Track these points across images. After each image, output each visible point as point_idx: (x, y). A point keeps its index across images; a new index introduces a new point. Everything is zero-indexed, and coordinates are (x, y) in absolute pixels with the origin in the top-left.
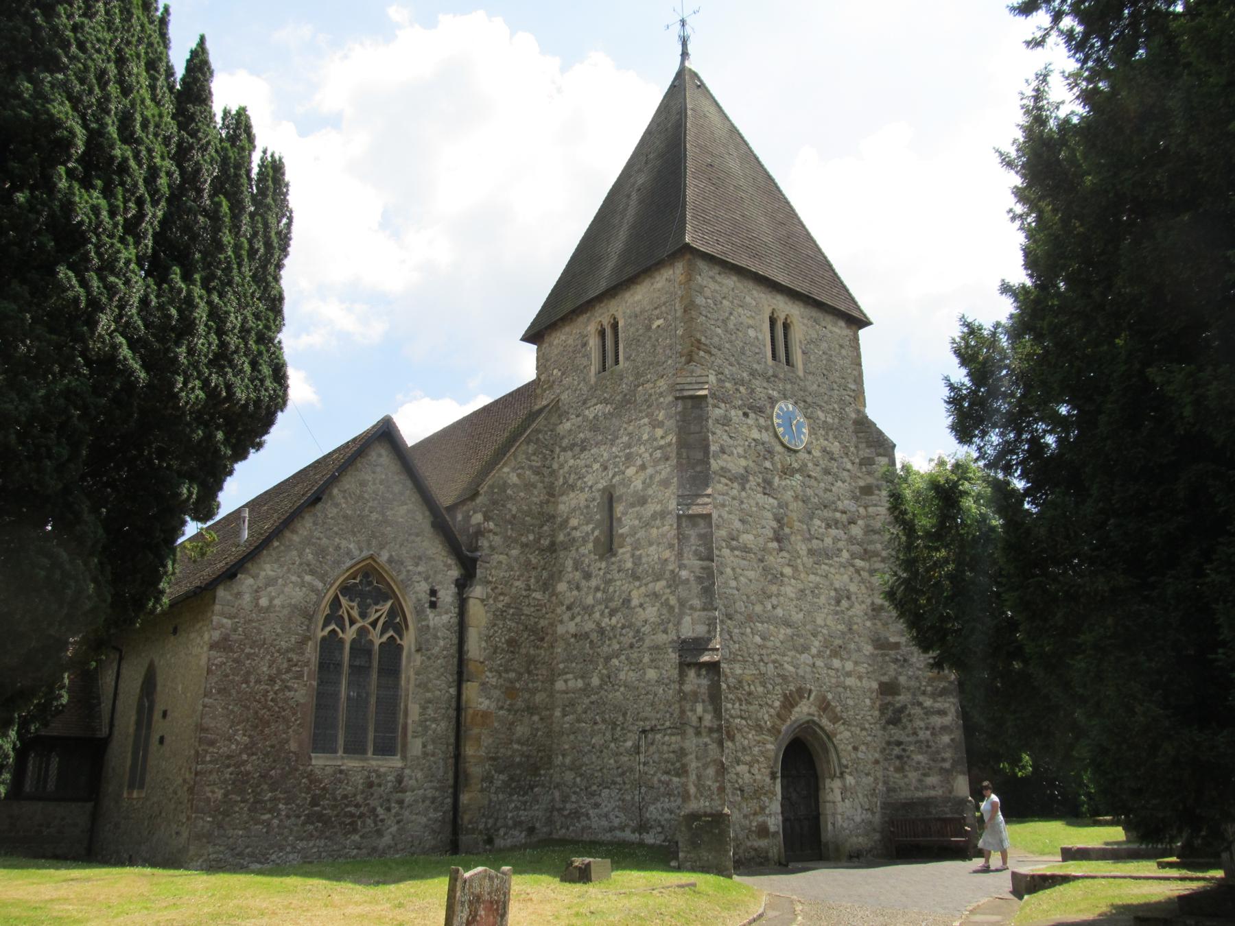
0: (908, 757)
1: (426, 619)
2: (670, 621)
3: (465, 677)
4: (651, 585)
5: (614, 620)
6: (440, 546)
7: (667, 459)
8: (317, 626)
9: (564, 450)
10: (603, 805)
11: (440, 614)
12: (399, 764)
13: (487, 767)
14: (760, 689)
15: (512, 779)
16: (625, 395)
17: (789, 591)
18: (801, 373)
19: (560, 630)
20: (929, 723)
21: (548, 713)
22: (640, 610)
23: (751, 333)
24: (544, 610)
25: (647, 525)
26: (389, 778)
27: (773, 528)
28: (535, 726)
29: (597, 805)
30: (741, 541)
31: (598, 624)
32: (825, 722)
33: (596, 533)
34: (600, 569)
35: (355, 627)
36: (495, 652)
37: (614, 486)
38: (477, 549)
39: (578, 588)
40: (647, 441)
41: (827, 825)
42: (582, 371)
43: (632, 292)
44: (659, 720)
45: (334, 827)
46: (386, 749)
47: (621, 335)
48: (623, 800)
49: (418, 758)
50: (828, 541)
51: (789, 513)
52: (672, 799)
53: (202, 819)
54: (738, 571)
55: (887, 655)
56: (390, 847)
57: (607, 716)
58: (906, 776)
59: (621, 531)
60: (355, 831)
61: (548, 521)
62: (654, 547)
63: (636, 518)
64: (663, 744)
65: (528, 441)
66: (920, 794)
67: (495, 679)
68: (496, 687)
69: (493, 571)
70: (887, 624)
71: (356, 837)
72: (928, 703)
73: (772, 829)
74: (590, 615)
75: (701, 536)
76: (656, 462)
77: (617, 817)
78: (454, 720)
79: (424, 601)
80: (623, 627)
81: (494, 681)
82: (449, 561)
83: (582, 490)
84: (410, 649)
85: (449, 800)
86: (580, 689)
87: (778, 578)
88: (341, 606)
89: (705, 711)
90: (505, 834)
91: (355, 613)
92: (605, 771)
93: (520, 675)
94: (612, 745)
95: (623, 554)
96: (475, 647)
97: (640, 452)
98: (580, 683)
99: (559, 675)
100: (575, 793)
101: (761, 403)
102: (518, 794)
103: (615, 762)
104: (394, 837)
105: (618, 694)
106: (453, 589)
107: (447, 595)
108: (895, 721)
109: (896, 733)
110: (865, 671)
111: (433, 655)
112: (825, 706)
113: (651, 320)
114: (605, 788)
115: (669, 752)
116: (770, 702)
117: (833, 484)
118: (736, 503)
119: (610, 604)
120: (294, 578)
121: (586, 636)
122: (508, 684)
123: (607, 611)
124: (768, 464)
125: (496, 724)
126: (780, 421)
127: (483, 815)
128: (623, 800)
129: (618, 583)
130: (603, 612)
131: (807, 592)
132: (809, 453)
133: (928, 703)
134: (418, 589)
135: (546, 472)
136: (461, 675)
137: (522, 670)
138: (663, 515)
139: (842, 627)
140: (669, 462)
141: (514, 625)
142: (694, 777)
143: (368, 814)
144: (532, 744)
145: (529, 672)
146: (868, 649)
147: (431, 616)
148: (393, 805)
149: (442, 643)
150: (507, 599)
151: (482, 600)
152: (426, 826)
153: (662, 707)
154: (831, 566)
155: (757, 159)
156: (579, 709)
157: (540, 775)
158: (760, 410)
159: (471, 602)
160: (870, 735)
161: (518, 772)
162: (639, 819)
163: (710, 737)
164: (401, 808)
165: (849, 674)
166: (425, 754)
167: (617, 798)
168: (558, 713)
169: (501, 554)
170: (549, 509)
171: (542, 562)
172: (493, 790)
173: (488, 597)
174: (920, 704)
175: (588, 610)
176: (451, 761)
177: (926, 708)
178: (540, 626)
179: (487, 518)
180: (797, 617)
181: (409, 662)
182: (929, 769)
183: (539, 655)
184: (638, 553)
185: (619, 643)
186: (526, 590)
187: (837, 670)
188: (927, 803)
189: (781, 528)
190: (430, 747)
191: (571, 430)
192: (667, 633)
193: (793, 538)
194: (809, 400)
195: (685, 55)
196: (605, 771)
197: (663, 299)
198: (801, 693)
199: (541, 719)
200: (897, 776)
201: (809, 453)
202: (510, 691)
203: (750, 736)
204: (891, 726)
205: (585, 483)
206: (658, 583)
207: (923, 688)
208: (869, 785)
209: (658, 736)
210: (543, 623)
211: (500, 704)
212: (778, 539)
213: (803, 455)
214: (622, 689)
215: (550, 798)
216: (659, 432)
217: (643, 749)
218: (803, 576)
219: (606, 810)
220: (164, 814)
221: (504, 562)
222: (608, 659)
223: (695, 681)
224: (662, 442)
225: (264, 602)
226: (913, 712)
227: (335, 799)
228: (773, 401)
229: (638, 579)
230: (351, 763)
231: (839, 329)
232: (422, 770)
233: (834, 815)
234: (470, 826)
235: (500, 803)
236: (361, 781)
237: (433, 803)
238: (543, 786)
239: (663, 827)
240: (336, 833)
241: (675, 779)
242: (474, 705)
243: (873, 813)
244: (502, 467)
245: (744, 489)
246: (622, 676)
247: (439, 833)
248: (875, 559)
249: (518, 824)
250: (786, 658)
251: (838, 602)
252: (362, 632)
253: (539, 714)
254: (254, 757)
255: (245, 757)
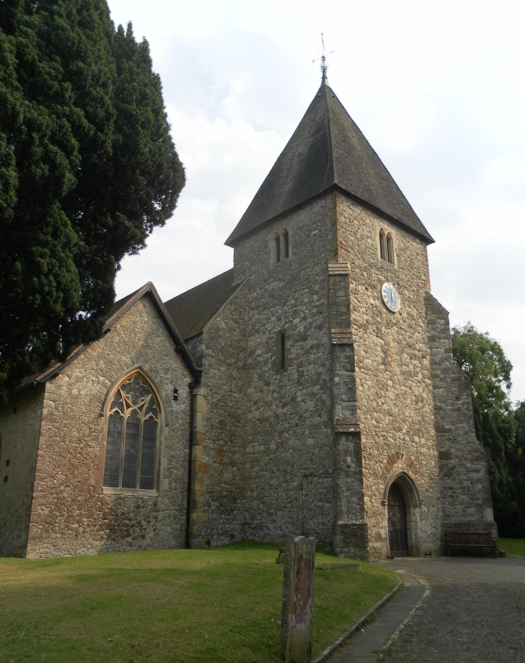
0: (457, 496)
1: (171, 406)
2: (323, 409)
3: (194, 442)
4: (310, 389)
5: (285, 410)
6: (180, 363)
7: (321, 313)
8: (107, 408)
9: (252, 309)
10: (278, 521)
11: (179, 404)
12: (155, 494)
13: (207, 497)
14: (376, 452)
15: (221, 505)
16: (293, 276)
17: (391, 394)
18: (396, 268)
19: (250, 416)
20: (469, 477)
21: (242, 466)
22: (303, 403)
23: (369, 240)
24: (240, 404)
25: (307, 352)
26: (149, 503)
27: (381, 357)
28: (234, 474)
29: (274, 521)
30: (364, 363)
31: (275, 413)
32: (410, 473)
33: (273, 358)
34: (276, 380)
35: (130, 409)
36: (212, 428)
37: (285, 330)
38: (201, 366)
39: (261, 391)
40: (307, 302)
41: (411, 536)
42: (264, 262)
43: (297, 214)
44: (315, 469)
45: (116, 533)
46: (147, 485)
47: (290, 240)
48: (291, 518)
49: (166, 491)
50: (411, 367)
51: (390, 349)
52: (324, 516)
53: (36, 526)
54: (363, 380)
55: (444, 436)
56: (149, 545)
57: (281, 467)
58: (455, 508)
59: (290, 357)
60: (129, 535)
61: (242, 351)
62: (312, 365)
63: (300, 349)
64: (318, 483)
65: (231, 303)
66: (463, 519)
67: (212, 444)
68: (212, 449)
69: (211, 379)
70: (444, 417)
71: (129, 539)
72: (469, 465)
73: (384, 536)
74: (269, 407)
75: (347, 357)
76: (314, 315)
77: (287, 528)
78: (187, 469)
79: (170, 395)
80: (291, 414)
81: (211, 445)
82: (185, 373)
83: (264, 333)
84: (162, 424)
85: (184, 517)
86: (263, 451)
87: (385, 387)
88: (121, 397)
89: (352, 461)
90: (217, 539)
91: (130, 402)
92: (279, 500)
93: (226, 442)
94: (284, 485)
95: (291, 370)
96: (200, 425)
97: (303, 309)
98: (263, 448)
99: (249, 443)
100: (259, 514)
101: (375, 283)
102: (225, 514)
103: (287, 494)
104: (152, 539)
105: (288, 453)
106: (187, 389)
107: (184, 393)
108: (448, 475)
109: (449, 482)
110: (431, 444)
111: (175, 428)
112: (411, 465)
113: (310, 231)
114: (280, 510)
115: (322, 488)
116: (381, 460)
117: (413, 334)
118: (362, 340)
119: (283, 400)
120: (94, 378)
121: (267, 420)
122: (219, 448)
123: (280, 404)
124: (379, 319)
125: (212, 471)
126: (385, 294)
127: (205, 527)
128: (291, 518)
129: (288, 388)
130: (278, 405)
131: (400, 396)
132: (401, 314)
133: (469, 465)
134: (167, 388)
135: (241, 322)
136: (192, 441)
137: (227, 440)
138: (318, 346)
139: (419, 418)
140: (322, 315)
141: (223, 412)
142: (345, 502)
143: (136, 525)
144: (233, 484)
145: (231, 441)
146: (433, 432)
147: (174, 405)
148: (152, 519)
149: (181, 422)
150: (219, 397)
151: (205, 396)
152: (171, 533)
153: (317, 461)
154: (413, 381)
155: (367, 142)
156: (262, 464)
157: (237, 503)
158: (374, 287)
159: (199, 397)
160: (434, 483)
161: (225, 501)
162: (302, 529)
163: (355, 477)
164: (156, 521)
165: (422, 446)
166: (170, 489)
167: (287, 516)
168: (248, 466)
169: (216, 369)
170: (243, 344)
171: (239, 376)
172: (210, 511)
173: (208, 395)
174: (464, 465)
175: (268, 404)
176: (186, 493)
177: (467, 468)
178: (237, 414)
179: (208, 348)
180: (395, 410)
181: (161, 432)
182: (470, 504)
183: (237, 431)
184: (301, 369)
185: (288, 423)
186: (230, 392)
187: (417, 443)
188: (469, 524)
189: (386, 357)
190: (173, 484)
191: (257, 297)
192: (321, 417)
193: (392, 364)
194: (400, 283)
195: (324, 78)
196: (279, 500)
197: (318, 218)
198: (398, 456)
199: (238, 469)
200: (450, 507)
201: (401, 314)
202: (220, 452)
203: (371, 479)
204: (447, 478)
205: (266, 328)
206: (315, 387)
207: (465, 456)
208: (434, 512)
209: (315, 479)
210: (239, 412)
211: (215, 459)
212: (384, 364)
213: (397, 315)
214: (291, 451)
215: (243, 517)
216: (315, 297)
217: (305, 487)
218: (398, 386)
219: (279, 524)
220: (8, 525)
221: (217, 374)
222: (281, 433)
223: (345, 443)
224: (318, 303)
225: (75, 392)
226: (459, 470)
227: (117, 516)
228: (381, 283)
229: (301, 384)
230: (127, 493)
231: (415, 245)
232: (168, 498)
233: (416, 529)
234: (197, 533)
235: (214, 519)
236: (133, 504)
237: (174, 519)
238: (239, 510)
239: (318, 533)
240: (118, 536)
241: (326, 505)
242: (200, 460)
243: (437, 529)
244: (216, 318)
245: (366, 333)
246: (291, 443)
247: (178, 537)
248: (437, 379)
249: (225, 533)
250: (389, 434)
251: (417, 403)
252: (134, 412)
253: (236, 466)
254: (68, 488)
255: (62, 488)
